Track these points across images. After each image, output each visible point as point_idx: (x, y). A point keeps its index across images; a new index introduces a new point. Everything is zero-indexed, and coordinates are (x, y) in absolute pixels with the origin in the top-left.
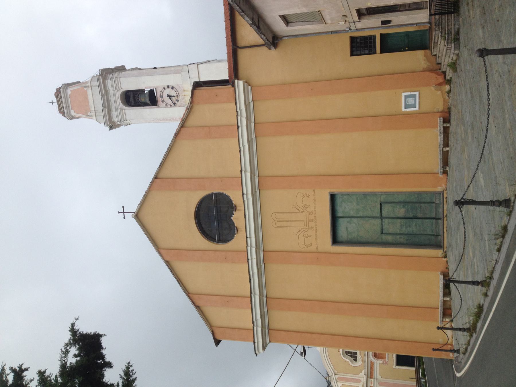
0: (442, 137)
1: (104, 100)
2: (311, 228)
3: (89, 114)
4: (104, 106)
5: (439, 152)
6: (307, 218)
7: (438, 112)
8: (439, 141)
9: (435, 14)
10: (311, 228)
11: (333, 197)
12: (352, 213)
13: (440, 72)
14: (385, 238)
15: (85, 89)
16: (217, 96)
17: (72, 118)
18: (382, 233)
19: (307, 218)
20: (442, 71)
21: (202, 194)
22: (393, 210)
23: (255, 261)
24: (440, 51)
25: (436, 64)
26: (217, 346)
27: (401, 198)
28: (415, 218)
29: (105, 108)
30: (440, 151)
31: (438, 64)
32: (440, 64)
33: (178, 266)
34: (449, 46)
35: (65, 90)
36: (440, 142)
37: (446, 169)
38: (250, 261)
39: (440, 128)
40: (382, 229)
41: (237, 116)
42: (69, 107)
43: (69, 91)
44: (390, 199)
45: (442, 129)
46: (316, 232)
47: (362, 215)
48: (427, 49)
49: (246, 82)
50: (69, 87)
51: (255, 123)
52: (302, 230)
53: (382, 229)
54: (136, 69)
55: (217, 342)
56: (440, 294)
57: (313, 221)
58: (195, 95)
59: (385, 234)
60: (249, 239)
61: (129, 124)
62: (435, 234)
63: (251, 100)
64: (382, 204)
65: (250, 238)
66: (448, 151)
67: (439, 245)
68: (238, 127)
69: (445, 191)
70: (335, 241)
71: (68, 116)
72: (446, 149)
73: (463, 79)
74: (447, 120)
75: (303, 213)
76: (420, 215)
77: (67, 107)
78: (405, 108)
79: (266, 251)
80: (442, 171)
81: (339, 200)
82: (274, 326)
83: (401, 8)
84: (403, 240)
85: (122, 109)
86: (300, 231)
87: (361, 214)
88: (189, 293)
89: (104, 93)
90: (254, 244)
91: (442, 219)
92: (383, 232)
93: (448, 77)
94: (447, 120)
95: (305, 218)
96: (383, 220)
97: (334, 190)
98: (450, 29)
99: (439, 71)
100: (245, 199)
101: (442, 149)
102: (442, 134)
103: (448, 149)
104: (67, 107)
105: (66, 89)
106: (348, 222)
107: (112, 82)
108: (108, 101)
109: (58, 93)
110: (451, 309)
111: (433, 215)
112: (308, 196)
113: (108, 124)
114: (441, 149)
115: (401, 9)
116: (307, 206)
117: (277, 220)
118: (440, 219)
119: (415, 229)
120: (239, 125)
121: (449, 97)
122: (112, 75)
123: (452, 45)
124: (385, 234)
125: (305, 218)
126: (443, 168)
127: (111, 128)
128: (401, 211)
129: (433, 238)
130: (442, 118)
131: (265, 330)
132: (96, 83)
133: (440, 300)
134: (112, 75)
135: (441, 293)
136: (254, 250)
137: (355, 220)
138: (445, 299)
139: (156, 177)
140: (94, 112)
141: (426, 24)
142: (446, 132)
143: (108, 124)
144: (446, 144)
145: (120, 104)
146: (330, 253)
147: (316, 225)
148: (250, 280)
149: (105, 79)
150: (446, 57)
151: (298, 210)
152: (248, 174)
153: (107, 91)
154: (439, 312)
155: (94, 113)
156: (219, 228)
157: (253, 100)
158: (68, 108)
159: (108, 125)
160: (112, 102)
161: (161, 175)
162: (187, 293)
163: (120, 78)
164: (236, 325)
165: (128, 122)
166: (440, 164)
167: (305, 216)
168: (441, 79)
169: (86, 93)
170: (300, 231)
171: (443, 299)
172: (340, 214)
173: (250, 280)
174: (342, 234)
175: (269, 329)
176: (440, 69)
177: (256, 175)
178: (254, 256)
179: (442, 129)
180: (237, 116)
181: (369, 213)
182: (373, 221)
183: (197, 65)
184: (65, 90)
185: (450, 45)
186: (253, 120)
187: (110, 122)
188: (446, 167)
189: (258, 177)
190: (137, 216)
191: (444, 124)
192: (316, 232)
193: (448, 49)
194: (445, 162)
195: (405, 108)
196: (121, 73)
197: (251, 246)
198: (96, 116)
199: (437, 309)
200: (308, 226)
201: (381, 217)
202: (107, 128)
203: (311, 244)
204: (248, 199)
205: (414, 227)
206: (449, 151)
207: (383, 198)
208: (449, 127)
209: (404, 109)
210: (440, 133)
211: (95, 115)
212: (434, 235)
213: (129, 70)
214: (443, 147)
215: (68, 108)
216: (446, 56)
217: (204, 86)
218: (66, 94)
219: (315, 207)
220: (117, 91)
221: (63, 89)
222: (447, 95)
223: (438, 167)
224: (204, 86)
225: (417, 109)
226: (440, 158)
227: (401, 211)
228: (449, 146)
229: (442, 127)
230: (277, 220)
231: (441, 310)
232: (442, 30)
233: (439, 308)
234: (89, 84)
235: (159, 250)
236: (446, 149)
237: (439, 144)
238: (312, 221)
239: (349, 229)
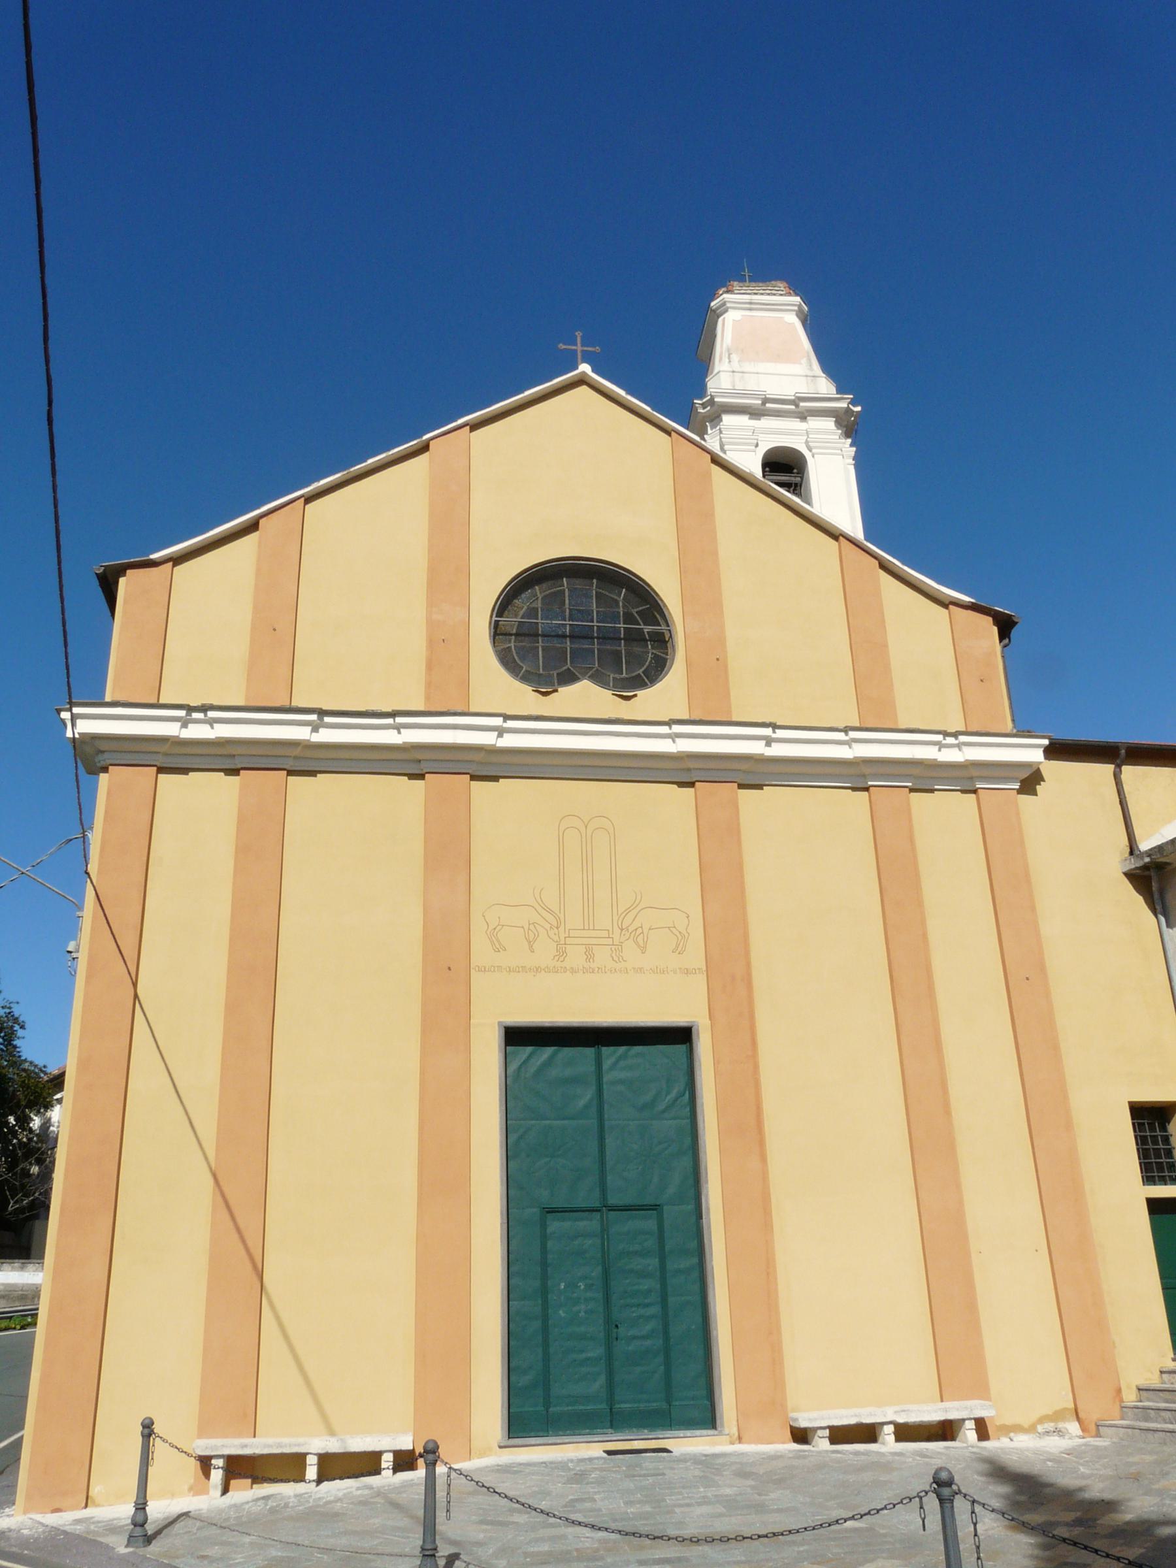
2: (561, 954)
10: (561, 954)
46: (548, 970)
86: (550, 912)
112: (679, 950)
170: (550, 912)
192: (548, 970)
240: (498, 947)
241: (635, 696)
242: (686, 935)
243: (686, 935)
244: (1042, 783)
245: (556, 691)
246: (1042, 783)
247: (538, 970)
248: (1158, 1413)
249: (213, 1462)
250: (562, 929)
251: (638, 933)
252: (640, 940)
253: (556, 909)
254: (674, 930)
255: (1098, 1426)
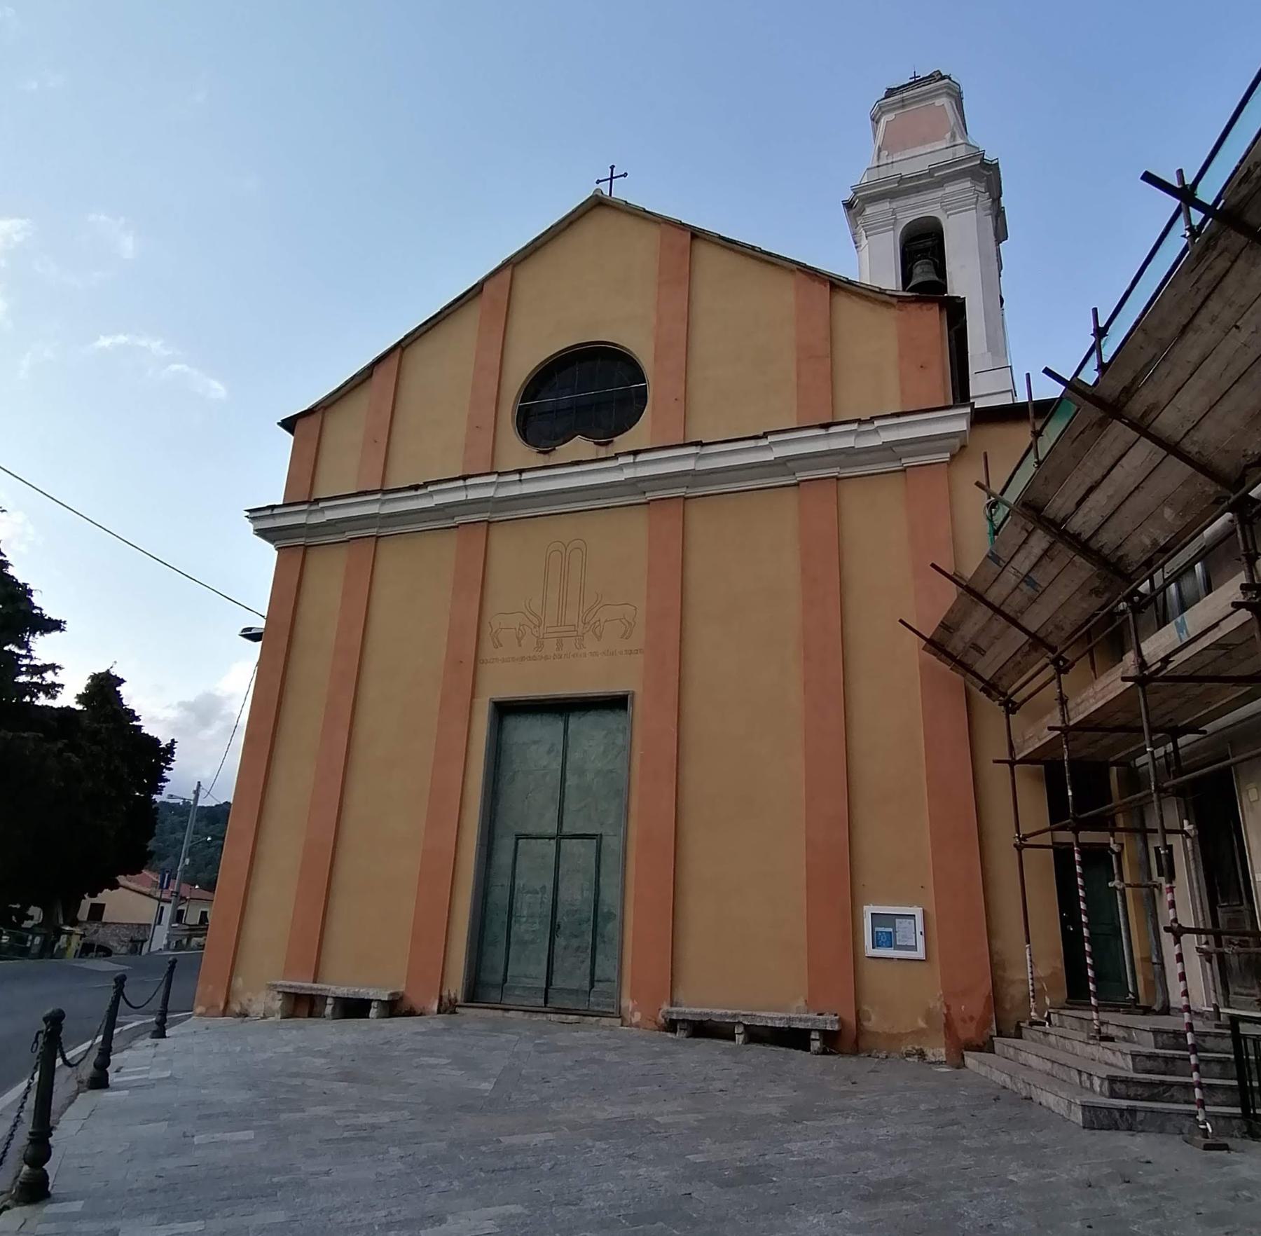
0: (778, 1024)
1: (919, 177)
2: (540, 645)
3: (884, 153)
4: (902, 180)
5: (729, 1012)
6: (565, 634)
7: (858, 1020)
8: (763, 1014)
9: (1237, 1038)
10: (540, 645)
11: (618, 703)
12: (574, 756)
13: (992, 1034)
14: (505, 845)
15: (948, 135)
16: (922, 367)
17: (875, 120)
18: (518, 837)
19: (565, 634)
20: (994, 1038)
21: (646, 360)
22: (578, 871)
23: (460, 496)
24: (1067, 1041)
25: (1018, 1022)
26: (278, 423)
27: (609, 895)
28: (554, 929)
29: (898, 182)
30: (735, 1016)
31: (1019, 1028)
32: (1019, 1036)
33: (471, 317)
34: (1097, 1082)
35: (945, 90)
36: (759, 1016)
37: (681, 1029)
38: (461, 483)
39: (807, 1020)
40: (528, 837)
41: (859, 421)
42: (903, 107)
43: (944, 101)
44: (608, 862)
45: (801, 1026)
46: (530, 658)
47: (568, 783)
48: (1070, 996)
49: (963, 447)
50: (954, 103)
51: (838, 479)
52: (536, 621)
53: (528, 837)
54: (1000, 267)
55: (289, 424)
56: (342, 989)
57: (558, 649)
58: (925, 307)
59: (517, 844)
60: (517, 477)
61: (856, 247)
62: (506, 985)
63: (906, 462)
64: (595, 841)
65: (520, 480)
66: (734, 1039)
67: (475, 993)
68: (826, 426)
69: (619, 1020)
70: (504, 710)
71: (880, 109)
72: (738, 1034)
73: (964, 1132)
74: (833, 1042)
75: (580, 622)
76: (560, 942)
77: (903, 103)
78: (872, 914)
79: (488, 530)
80: (674, 1017)
81: (611, 719)
82: (314, 558)
83: (1224, 913)
84: (499, 895)
85: (894, 224)
86: (535, 615)
87: (571, 781)
88: (403, 350)
89: (936, 175)
90: (504, 493)
91: (545, 1006)
92: (520, 841)
93: (974, 1058)
94: (833, 1042)
95: (567, 628)
96: (553, 842)
97: (638, 707)
98: (1172, 1096)
99: (995, 1029)
100: (621, 460)
101: (739, 1023)
102: (786, 1026)
103: (740, 1039)
104: (903, 101)
105: (949, 95)
106: (553, 745)
107: (965, 191)
108: (918, 190)
109: (937, 76)
110: (310, 1015)
111: (558, 982)
112: (625, 636)
113: (858, 195)
114: (741, 1019)
115: (1219, 911)
116: (598, 634)
117: (568, 554)
118: (546, 1002)
119: (523, 927)
120: (833, 430)
121: (908, 1055)
122: (983, 190)
123: (1102, 1094)
124: (517, 844)
125: (567, 628)
126: (683, 1021)
127: (849, 205)
128: (575, 893)
129: (499, 978)
130: (836, 1027)
131: (302, 537)
132: (961, 152)
133: (328, 987)
134: (983, 190)
135: (345, 991)
136: (489, 492)
137: (557, 765)
138: (330, 1001)
139: (696, 235)
140: (890, 161)
141: (1160, 998)
142: (794, 1038)
143: (858, 195)
144: (759, 1035)
145: (907, 217)
146: (473, 697)
147: (546, 658)
148: (416, 488)
149: (971, 174)
150: (1049, 1064)
151: (591, 609)
152: (688, 465)
153: (941, 183)
154: (305, 984)
155: (885, 162)
156: (557, 411)
157: (908, 470)
158: (901, 104)
159: (855, 193)
160: (913, 200)
161: (703, 249)
162: (403, 344)
163: (976, 208)
164: (324, 467)
165: (864, 242)
166: (696, 1014)
167: (572, 628)
168: (967, 1032)
169: (940, 138)
170: (535, 615)
171: (330, 995)
172: (575, 722)
173: (416, 488)
174: (524, 730)
175: (306, 547)
176: (1000, 1034)
177: (689, 491)
178: (473, 494)
179: (803, 1027)
180: (859, 421)
181: (571, 805)
182: (552, 814)
183: (1011, 391)
184: (945, 90)
185: (1101, 1087)
186: (847, 472)
187: (863, 200)
188: (685, 1030)
189: (683, 496)
190: (597, 203)
191: (818, 1034)
192: (530, 658)
193: (1085, 1077)
194: (702, 1029)
195: (872, 914)
196: (989, 212)
197: (499, 485)
198: (878, 166)
199: (312, 978)
200: (546, 636)
201: (559, 837)
202: (848, 196)
203: (498, 645)
204: (621, 467)
205: (530, 927)
206: (732, 1043)
207: (612, 843)
208: (807, 1048)
209: (868, 910)
210: (790, 1019)
211: (881, 164)
212: (505, 980)
213: (998, 251)
214: (745, 1025)
215: (901, 104)
216: (1053, 1062)
217: (951, 333)
218: (934, 94)
219: (595, 654)
220: (942, 207)
221: (947, 86)
222: (914, 1048)
223: (690, 1009)
224: (951, 333)
225: (870, 951)
226: (711, 1014)
227: (575, 893)
228: (749, 1046)
229: (809, 1025)
230: (568, 554)
231: (312, 989)
232: (1160, 1060)
233: (315, 982)
234: (959, 141)
235: (511, 266)
236: (738, 1034)
237: (754, 1013)
238: (560, 645)
239: (534, 747)
240: (591, 622)
241: (612, 441)
242: (633, 624)
243: (633, 624)
244: (76, 700)
245: (554, 449)
246: (76, 700)
247: (523, 658)
248: (930, 1068)
249: (373, 1004)
250: (541, 628)
251: (597, 624)
252: (597, 630)
253: (539, 614)
254: (623, 620)
255: (620, 1017)
